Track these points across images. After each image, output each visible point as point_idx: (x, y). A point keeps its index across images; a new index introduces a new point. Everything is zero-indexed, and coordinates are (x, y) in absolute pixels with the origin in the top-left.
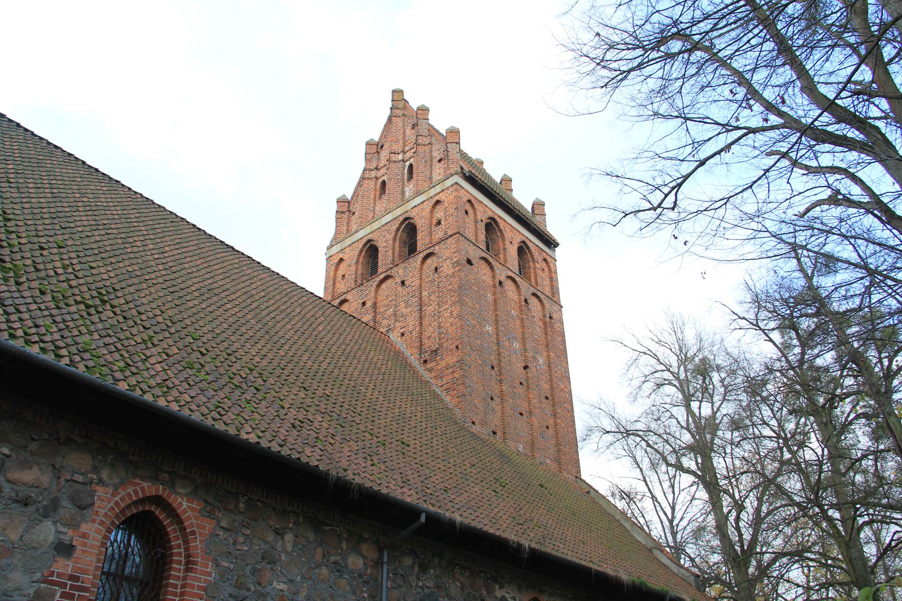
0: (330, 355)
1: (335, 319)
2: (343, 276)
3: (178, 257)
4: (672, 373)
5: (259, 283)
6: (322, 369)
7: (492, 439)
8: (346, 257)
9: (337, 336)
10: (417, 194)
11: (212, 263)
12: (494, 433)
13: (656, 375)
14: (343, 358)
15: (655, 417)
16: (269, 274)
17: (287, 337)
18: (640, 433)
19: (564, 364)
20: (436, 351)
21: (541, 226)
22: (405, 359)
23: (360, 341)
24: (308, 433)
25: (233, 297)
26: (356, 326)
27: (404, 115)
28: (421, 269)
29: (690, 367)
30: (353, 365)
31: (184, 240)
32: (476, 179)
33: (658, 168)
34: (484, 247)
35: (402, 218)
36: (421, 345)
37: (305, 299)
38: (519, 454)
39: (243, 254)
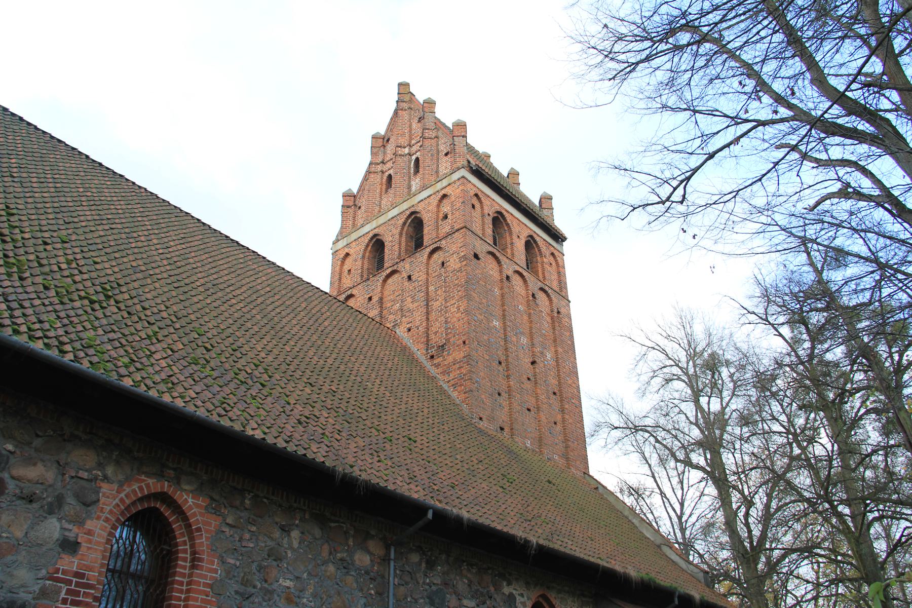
0: (336, 350)
1: (341, 315)
3: (182, 252)
4: (681, 368)
5: (264, 278)
6: (328, 365)
7: (499, 435)
8: (352, 252)
9: (343, 331)
10: (424, 188)
11: (216, 258)
13: (665, 370)
15: (664, 413)
16: (275, 269)
17: (293, 332)
18: (649, 429)
19: (572, 359)
20: (443, 346)
22: (412, 354)
25: (238, 292)
26: (362, 321)
28: (428, 264)
29: (699, 362)
30: (360, 361)
31: (189, 235)
33: (666, 161)
35: (408, 213)
36: (428, 341)
37: (310, 294)
38: (526, 450)
39: (248, 249)
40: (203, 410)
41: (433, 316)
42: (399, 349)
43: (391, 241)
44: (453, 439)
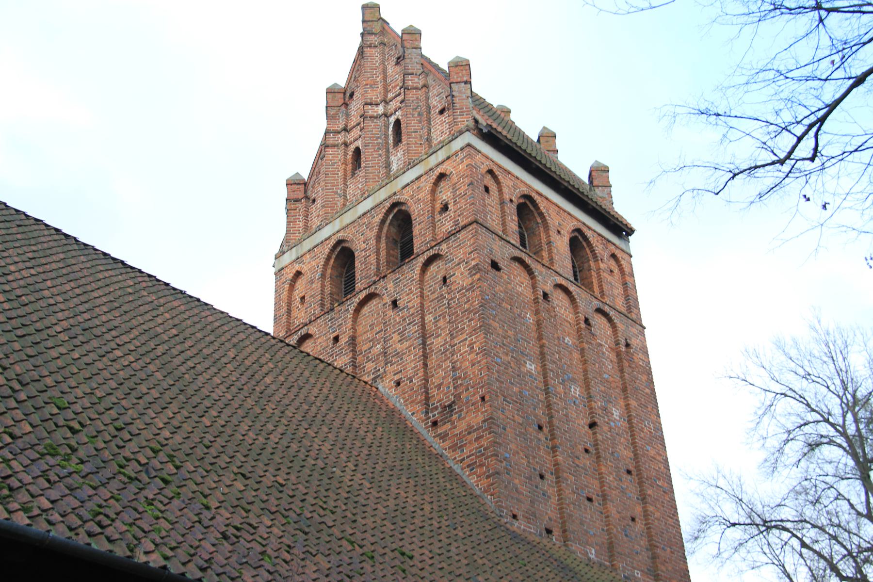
0: (284, 421)
1: (292, 366)
2: (303, 298)
3: (30, 280)
4: (832, 425)
5: (167, 316)
6: (271, 444)
7: (545, 541)
8: (305, 268)
9: (294, 390)
10: (410, 165)
11: (89, 288)
12: (549, 532)
13: (807, 429)
14: (305, 424)
15: (811, 498)
16: (184, 301)
17: (215, 396)
18: (789, 525)
19: (654, 417)
20: (450, 406)
21: (605, 204)
22: (403, 421)
23: (332, 397)
24: (249, 545)
25: (125, 338)
26: (324, 374)
27: (385, 46)
28: (422, 280)
29: (862, 414)
30: (321, 435)
31: (41, 254)
32: (499, 136)
33: (783, 95)
34: (515, 240)
35: (388, 204)
36: (427, 399)
37: (242, 336)
38: (589, 563)
39: (140, 271)
40: (62, 528)
41: (433, 361)
42: (383, 414)
43: (365, 250)
44: (471, 551)
